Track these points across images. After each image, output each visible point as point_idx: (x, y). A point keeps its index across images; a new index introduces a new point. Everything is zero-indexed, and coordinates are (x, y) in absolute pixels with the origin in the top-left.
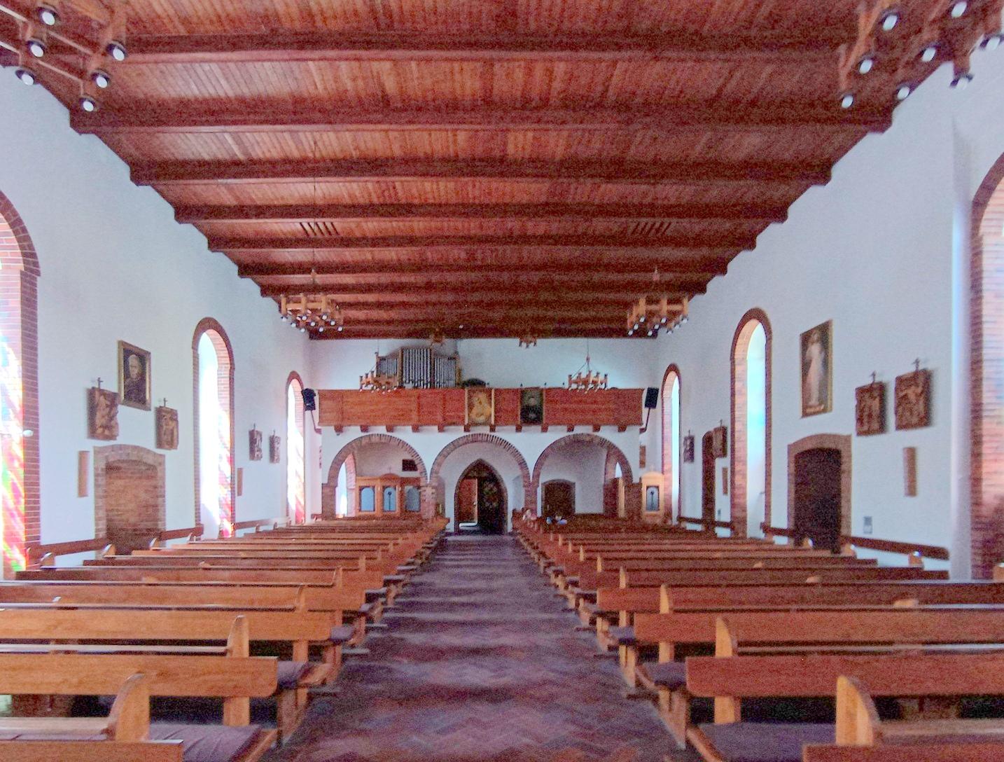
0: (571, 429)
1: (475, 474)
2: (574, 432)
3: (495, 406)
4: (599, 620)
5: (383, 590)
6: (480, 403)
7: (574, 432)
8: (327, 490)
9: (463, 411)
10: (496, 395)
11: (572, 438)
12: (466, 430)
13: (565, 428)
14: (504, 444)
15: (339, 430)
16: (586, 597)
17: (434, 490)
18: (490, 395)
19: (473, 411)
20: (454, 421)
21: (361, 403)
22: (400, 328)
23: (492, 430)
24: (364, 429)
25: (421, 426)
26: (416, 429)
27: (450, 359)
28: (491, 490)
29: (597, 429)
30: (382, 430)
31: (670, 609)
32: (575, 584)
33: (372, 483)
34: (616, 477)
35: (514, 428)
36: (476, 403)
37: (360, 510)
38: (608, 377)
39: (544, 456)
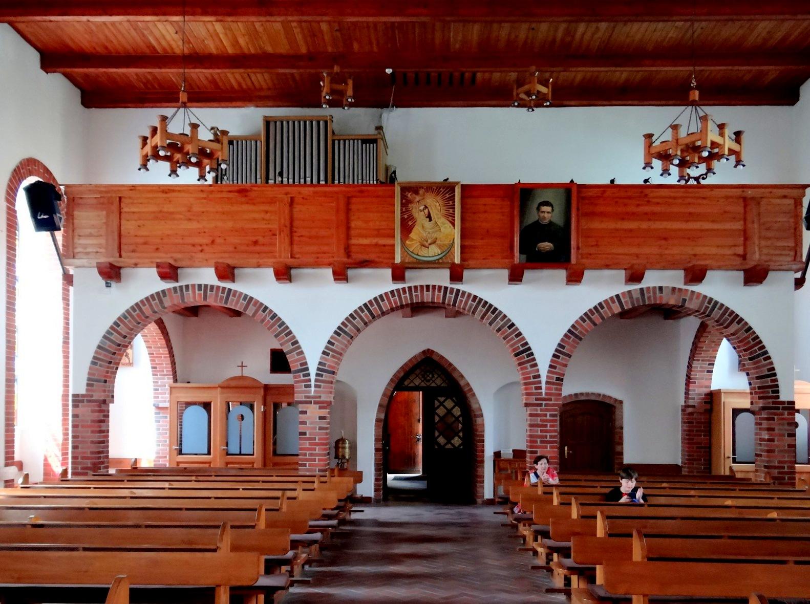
0: (635, 277)
1: (417, 382)
2: (644, 285)
3: (463, 220)
4: (574, 578)
5: (290, 554)
6: (429, 217)
7: (644, 285)
8: (86, 411)
9: (393, 236)
10: (463, 198)
11: (636, 295)
12: (398, 276)
13: (622, 274)
14: (481, 310)
15: (111, 273)
16: (559, 550)
17: (324, 412)
18: (452, 198)
19: (413, 235)
20: (372, 257)
21: (160, 216)
22: (260, 78)
23: (456, 276)
24: (169, 272)
25: (299, 267)
26: (284, 274)
27: (365, 141)
28: (449, 412)
29: (696, 275)
30: (207, 276)
31: (606, 533)
32: (546, 535)
33: (204, 397)
34: (714, 387)
35: (505, 273)
36: (420, 217)
37: (180, 452)
38: (744, 138)
39: (573, 335)
